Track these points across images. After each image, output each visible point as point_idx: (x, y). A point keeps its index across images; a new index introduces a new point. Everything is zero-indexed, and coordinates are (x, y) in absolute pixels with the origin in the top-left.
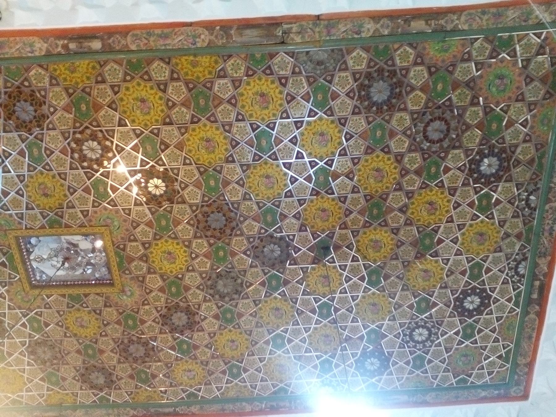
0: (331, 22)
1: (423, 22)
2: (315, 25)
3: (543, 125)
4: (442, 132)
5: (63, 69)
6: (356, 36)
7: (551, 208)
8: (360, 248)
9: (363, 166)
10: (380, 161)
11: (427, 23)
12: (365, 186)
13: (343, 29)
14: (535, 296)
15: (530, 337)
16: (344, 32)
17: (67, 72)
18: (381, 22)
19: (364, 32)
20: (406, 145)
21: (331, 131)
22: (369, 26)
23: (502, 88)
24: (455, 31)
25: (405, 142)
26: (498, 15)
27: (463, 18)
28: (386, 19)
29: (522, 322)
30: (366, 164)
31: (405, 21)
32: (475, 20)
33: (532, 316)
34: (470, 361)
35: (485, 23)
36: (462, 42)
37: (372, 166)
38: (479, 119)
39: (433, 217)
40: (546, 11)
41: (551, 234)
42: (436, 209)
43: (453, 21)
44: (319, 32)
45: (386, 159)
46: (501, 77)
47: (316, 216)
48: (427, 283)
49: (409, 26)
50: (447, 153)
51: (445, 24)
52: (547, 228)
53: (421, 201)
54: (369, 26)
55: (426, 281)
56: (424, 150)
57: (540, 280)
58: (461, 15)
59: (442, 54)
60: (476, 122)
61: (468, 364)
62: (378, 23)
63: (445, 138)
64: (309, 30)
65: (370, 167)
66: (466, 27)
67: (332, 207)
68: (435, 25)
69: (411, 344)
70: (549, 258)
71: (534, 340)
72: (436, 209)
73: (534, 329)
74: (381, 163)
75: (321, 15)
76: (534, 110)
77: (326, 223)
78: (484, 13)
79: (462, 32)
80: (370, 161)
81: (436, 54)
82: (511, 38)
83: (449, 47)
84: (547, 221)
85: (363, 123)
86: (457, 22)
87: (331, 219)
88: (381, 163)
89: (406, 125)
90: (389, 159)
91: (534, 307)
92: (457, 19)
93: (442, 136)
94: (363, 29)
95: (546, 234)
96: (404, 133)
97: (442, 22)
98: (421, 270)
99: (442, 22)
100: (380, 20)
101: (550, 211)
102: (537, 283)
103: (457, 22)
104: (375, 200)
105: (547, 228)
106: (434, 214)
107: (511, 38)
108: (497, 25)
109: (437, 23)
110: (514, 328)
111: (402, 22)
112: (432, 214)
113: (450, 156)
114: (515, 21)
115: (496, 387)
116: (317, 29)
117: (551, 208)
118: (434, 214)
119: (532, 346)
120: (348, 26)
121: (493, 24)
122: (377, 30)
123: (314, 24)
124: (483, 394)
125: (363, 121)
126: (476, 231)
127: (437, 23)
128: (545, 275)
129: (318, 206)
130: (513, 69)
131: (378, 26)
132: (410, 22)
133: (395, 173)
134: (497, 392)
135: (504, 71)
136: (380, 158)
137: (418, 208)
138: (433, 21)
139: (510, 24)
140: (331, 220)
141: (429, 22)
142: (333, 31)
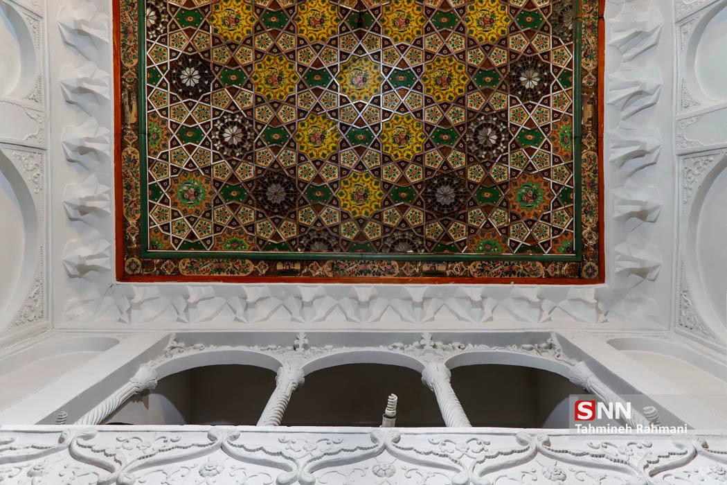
0: (596, 30)
1: (590, 117)
2: (595, 14)
3: (485, 245)
4: (485, 143)
5: (154, 146)
6: (583, 53)
7: (393, 267)
8: (358, 62)
9: (455, 64)
10: (459, 81)
11: (589, 119)
12: (433, 66)
13: (590, 41)
14: (280, 267)
15: (219, 270)
16: (588, 42)
17: (157, 142)
18: (593, 77)
19: (586, 60)
20: (474, 108)
21: (494, 31)
22: (591, 65)
23: (525, 198)
24: (581, 147)
25: (478, 106)
26: (592, 185)
27: (592, 153)
28: (595, 81)
29: (243, 257)
30: (457, 67)
31: (593, 99)
32: (589, 165)
33: (251, 269)
34: (189, 200)
35: (586, 174)
36: (570, 155)
37: (454, 73)
38: (495, 179)
39: (391, 141)
40: (592, 229)
41: (361, 272)
42: (399, 144)
43: (589, 143)
44: (589, 17)
45: (460, 87)
46: (535, 197)
47: (401, 13)
48: (306, 140)
49: (588, 103)
50: (462, 150)
51: (587, 136)
52: (369, 267)
53: (410, 127)
54: (591, 65)
55: (309, 138)
56: (468, 125)
57: (302, 269)
58: (594, 151)
59: (560, 136)
60: (493, 176)
61: (183, 197)
62: (593, 74)
63: (479, 146)
64: (591, 8)
65: (453, 71)
66: (584, 156)
67: (410, 31)
68: (588, 127)
69: (219, 125)
70: (331, 275)
71: (217, 274)
72: (399, 144)
73: (232, 272)
74: (456, 83)
75: (604, 20)
76: (501, 233)
77: (391, 24)
78: (595, 172)
79: (579, 153)
80: (460, 71)
81: (561, 131)
82: (571, 201)
83: (566, 144)
84: (377, 266)
85: (500, 63)
86: (589, 148)
87: (397, 29)
88: (456, 83)
89: (495, 106)
90: (460, 91)
91: (265, 267)
92: (591, 148)
93: (481, 143)
94: (588, 59)
95: (361, 267)
96: (488, 105)
97: (590, 134)
98: (324, 132)
99: (590, 134)
100: (595, 76)
101: (389, 267)
102: (298, 267)
103: (589, 148)
104: (474, 80)
105: (369, 267)
106: (394, 142)
107: (571, 201)
108: (136, 32)
109: (590, 129)
110: (235, 249)
111: (592, 96)
112: (394, 139)
113: (460, 153)
114: (586, 201)
115: (141, 239)
116: (591, 16)
117: (393, 267)
118: (394, 142)
119: (207, 274)
120: (592, 45)
121: (135, 36)
122: (587, 72)
123: (596, 13)
124: (132, 222)
125: (502, 62)
126: (371, 189)
127: (590, 129)
128: (308, 273)
129: (412, 15)
130: (542, 207)
131: (590, 74)
132: (592, 103)
133: (444, 98)
134: (134, 238)
135: (540, 198)
136: (462, 82)
137: (403, 124)
138: (591, 125)
139: (584, 197)
140: (395, 29)
141: (590, 122)
142: (589, 31)
